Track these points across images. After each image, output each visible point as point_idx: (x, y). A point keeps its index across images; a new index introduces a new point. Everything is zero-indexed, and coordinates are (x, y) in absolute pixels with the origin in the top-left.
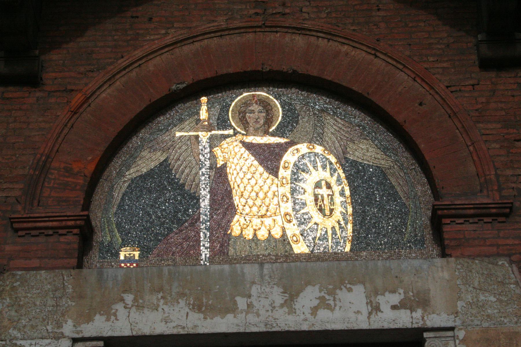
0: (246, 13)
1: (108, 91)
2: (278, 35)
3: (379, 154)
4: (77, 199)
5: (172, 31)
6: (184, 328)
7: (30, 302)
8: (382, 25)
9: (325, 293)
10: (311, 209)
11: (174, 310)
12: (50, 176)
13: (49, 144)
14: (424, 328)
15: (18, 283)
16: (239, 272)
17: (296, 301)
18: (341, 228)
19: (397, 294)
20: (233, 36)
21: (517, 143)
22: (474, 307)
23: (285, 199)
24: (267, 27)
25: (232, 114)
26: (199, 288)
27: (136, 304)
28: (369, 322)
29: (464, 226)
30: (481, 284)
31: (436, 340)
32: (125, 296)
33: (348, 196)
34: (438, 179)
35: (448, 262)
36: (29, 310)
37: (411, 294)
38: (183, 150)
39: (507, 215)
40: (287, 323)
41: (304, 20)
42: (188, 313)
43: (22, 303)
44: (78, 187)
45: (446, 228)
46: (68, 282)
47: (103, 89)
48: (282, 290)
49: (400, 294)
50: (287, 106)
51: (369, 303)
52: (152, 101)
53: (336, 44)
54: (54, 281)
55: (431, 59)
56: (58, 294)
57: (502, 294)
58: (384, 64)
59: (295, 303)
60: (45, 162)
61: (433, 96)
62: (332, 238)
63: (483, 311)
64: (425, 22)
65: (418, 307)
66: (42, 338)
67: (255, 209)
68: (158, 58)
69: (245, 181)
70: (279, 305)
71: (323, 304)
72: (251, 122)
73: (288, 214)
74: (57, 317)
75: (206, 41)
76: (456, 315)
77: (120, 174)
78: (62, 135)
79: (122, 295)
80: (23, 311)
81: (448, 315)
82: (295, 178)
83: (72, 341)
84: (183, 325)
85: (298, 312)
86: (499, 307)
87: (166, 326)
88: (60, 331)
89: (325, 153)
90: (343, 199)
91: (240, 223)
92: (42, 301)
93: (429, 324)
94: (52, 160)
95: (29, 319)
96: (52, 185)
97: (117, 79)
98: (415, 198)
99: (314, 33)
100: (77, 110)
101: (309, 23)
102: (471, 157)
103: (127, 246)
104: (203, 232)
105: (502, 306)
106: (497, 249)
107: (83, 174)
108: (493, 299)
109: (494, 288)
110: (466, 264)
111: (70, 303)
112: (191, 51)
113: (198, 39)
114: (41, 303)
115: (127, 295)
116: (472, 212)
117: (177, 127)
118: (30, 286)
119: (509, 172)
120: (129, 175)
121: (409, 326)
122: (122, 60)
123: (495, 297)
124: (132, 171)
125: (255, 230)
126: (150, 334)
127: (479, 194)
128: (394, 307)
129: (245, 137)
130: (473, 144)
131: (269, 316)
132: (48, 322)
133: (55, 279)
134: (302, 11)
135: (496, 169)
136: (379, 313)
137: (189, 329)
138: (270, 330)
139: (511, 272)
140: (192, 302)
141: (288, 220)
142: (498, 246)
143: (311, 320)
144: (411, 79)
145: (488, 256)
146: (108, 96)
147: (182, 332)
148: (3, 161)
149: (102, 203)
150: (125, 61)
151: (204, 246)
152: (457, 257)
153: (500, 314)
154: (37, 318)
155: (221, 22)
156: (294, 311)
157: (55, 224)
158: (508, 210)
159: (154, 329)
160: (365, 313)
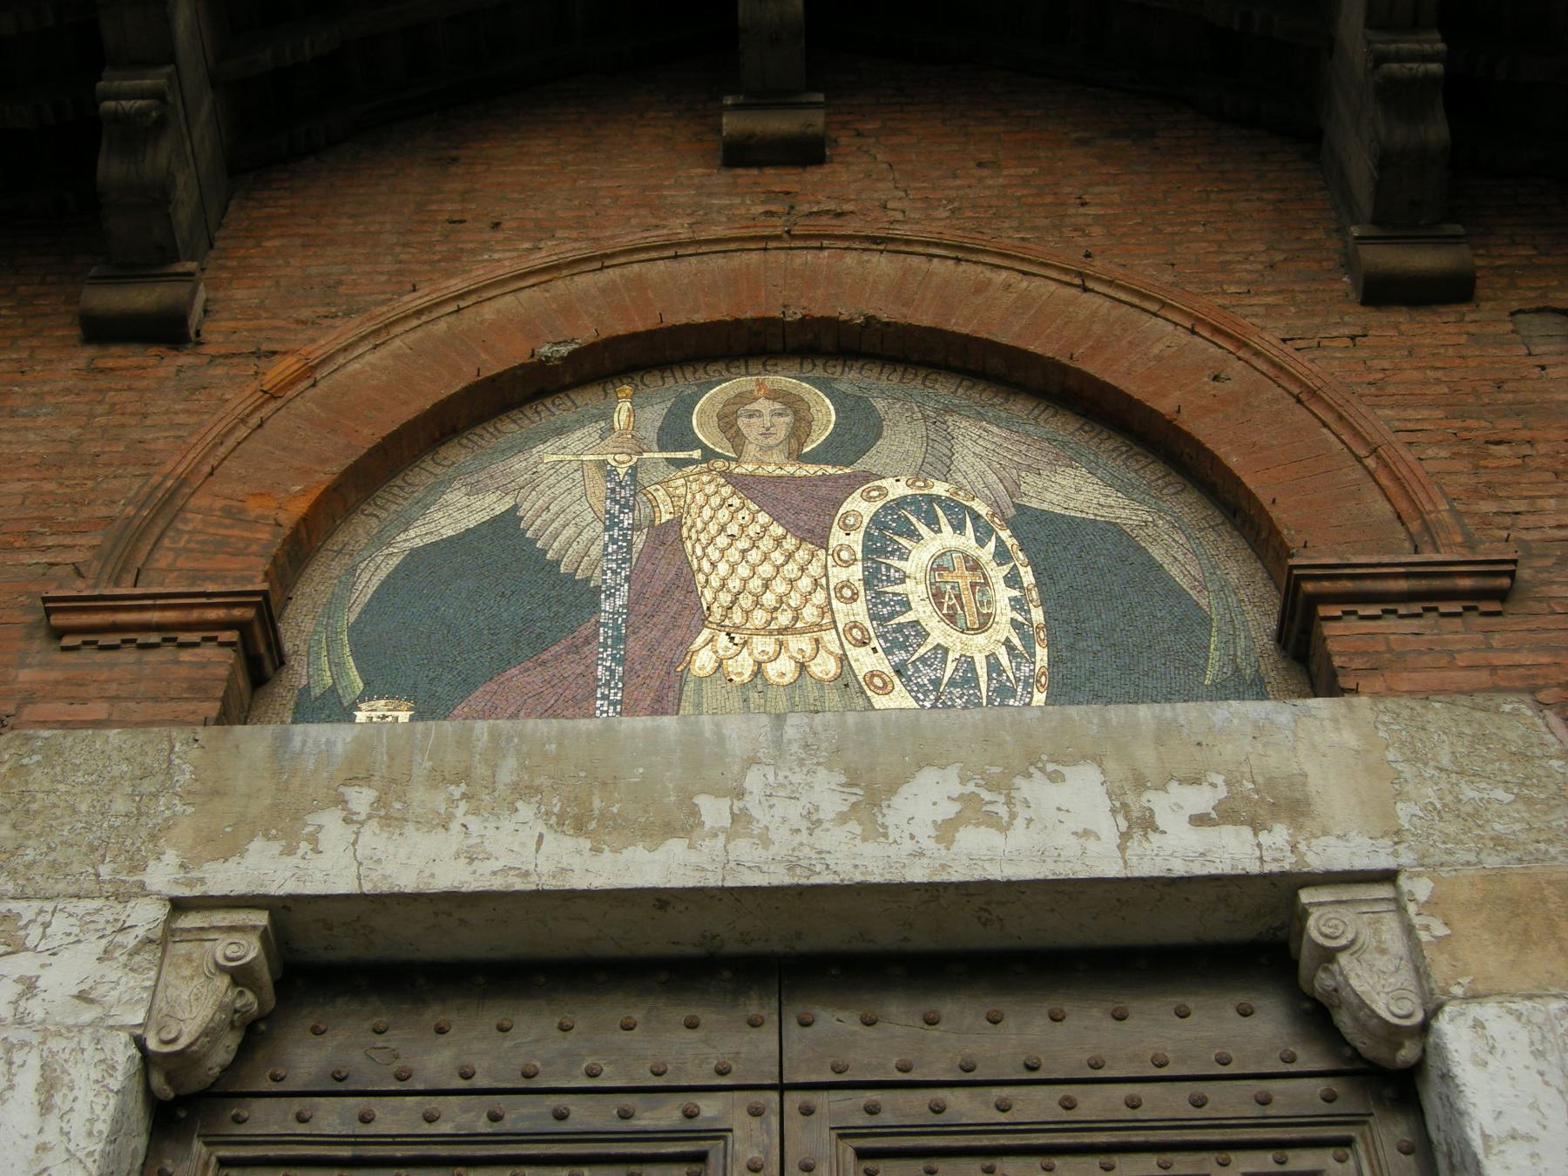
0: (743, 211)
1: (369, 358)
2: (826, 253)
4: (245, 573)
5: (549, 243)
6: (527, 874)
7: (62, 804)
8: (1097, 231)
9: (977, 785)
11: (497, 828)
12: (181, 526)
13: (190, 456)
14: (1300, 875)
15: (36, 758)
16: (708, 734)
17: (889, 806)
19: (1205, 787)
20: (705, 258)
24: (794, 237)
26: (583, 774)
27: (382, 813)
28: (1123, 858)
31: (1342, 909)
32: (351, 793)
33: (1031, 586)
34: (1288, 529)
35: (1351, 708)
36: (54, 823)
39: (1502, 595)
42: (541, 836)
43: (35, 806)
44: (254, 548)
46: (184, 756)
47: (356, 353)
48: (844, 779)
49: (1214, 785)
52: (485, 374)
53: (979, 268)
54: (144, 753)
55: (1233, 289)
56: (147, 786)
57: (1528, 782)
58: (1107, 303)
59: (885, 811)
60: (173, 493)
61: (1247, 362)
62: (990, 679)
64: (1204, 225)
65: (1275, 817)
66: (78, 897)
68: (508, 298)
70: (833, 815)
71: (972, 811)
74: (133, 844)
75: (636, 266)
76: (1396, 839)
77: (381, 540)
78: (231, 442)
79: (342, 789)
80: (35, 827)
81: (1371, 838)
83: (169, 907)
84: (524, 868)
85: (893, 833)
86: (1526, 815)
87: (471, 869)
88: (135, 878)
90: (1016, 593)
92: (95, 803)
93: (1316, 862)
94: (194, 493)
95: (49, 847)
96: (182, 544)
97: (396, 336)
99: (920, 249)
100: (281, 389)
101: (907, 227)
105: (1534, 814)
106: (1491, 675)
107: (272, 522)
108: (1500, 794)
109: (1500, 770)
110: (1406, 713)
111: (179, 808)
112: (596, 284)
114: (94, 807)
115: (357, 789)
117: (549, 444)
118: (69, 766)
119: (1488, 507)
120: (405, 541)
121: (1254, 868)
123: (1507, 790)
124: (412, 533)
125: (759, 664)
126: (416, 891)
128: (1199, 820)
129: (733, 465)
130: (1375, 450)
131: (802, 844)
132: (104, 856)
133: (148, 748)
134: (885, 207)
135: (1451, 501)
136: (1153, 836)
137: (544, 879)
138: (803, 881)
139: (1544, 729)
140: (556, 810)
141: (857, 640)
142: (1493, 669)
143: (936, 855)
144: (1183, 330)
145: (1470, 693)
146: (368, 368)
147: (519, 885)
149: (319, 602)
152: (1376, 695)
153: (1533, 835)
154: (71, 846)
155: (680, 228)
156: (881, 830)
157: (171, 616)
158: (1505, 582)
159: (432, 875)
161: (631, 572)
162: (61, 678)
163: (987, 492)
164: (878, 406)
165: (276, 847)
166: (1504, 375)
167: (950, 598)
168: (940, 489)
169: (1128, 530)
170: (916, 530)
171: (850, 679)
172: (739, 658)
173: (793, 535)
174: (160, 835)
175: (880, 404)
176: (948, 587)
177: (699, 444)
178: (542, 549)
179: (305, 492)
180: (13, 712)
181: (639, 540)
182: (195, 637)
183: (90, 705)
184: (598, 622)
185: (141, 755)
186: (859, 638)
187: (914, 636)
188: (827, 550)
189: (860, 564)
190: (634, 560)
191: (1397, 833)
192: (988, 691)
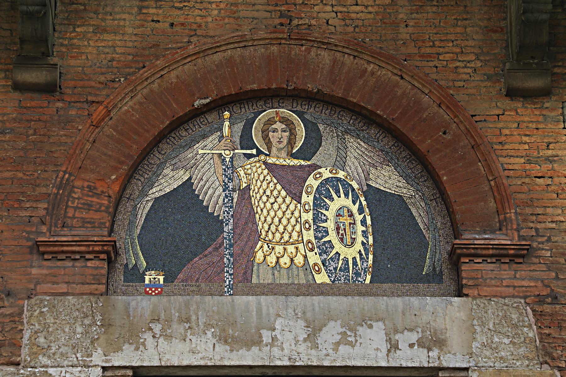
1: (130, 103)
3: (401, 182)
7: (59, 328)
9: (346, 329)
10: (332, 237)
12: (74, 195)
18: (361, 259)
21: (537, 179)
22: (488, 348)
23: (307, 226)
25: (255, 131)
27: (164, 334)
29: (481, 265)
30: (496, 326)
37: (429, 333)
38: (206, 169)
39: (523, 256)
40: (309, 357)
41: (330, 33)
43: (50, 329)
44: (103, 208)
45: (463, 268)
49: (418, 332)
50: (311, 128)
51: (389, 340)
53: (362, 62)
56: (87, 322)
58: (410, 87)
62: (353, 268)
63: (497, 353)
67: (278, 236)
69: (268, 205)
71: (344, 340)
72: (274, 141)
73: (310, 242)
75: (229, 51)
76: (470, 356)
77: (144, 194)
82: (319, 204)
85: (320, 346)
86: (512, 349)
89: (347, 178)
90: (364, 229)
91: (263, 250)
93: (445, 364)
95: (59, 347)
96: (75, 205)
98: (434, 231)
102: (492, 193)
103: (152, 270)
104: (227, 258)
108: (506, 341)
109: (508, 331)
110: (482, 305)
113: (221, 49)
114: (70, 330)
116: (491, 252)
117: (200, 144)
122: (144, 69)
124: (154, 190)
127: (498, 232)
129: (268, 158)
130: (495, 179)
132: (77, 350)
136: (398, 352)
139: (525, 315)
141: (310, 248)
142: (515, 287)
148: (25, 178)
149: (125, 224)
150: (147, 71)
151: (228, 272)
153: (513, 357)
157: (83, 249)
158: (525, 252)
160: (385, 351)
161: (233, 213)
162: (47, 273)
163: (358, 177)
164: (321, 129)
165: (133, 347)
166: (551, 140)
167: (342, 230)
168: (341, 174)
169: (405, 199)
170: (332, 195)
171: (308, 267)
172: (271, 255)
173: (289, 196)
174: (94, 342)
175: (321, 127)
176: (342, 224)
177: (254, 146)
178: (201, 200)
179: (117, 179)
180: (34, 288)
181: (236, 196)
182: (91, 256)
183: (60, 285)
184: (223, 237)
185: (82, 308)
186: (311, 247)
187: (329, 248)
188: (301, 204)
189: (312, 211)
190: (234, 207)
191: (471, 354)
192: (352, 274)
